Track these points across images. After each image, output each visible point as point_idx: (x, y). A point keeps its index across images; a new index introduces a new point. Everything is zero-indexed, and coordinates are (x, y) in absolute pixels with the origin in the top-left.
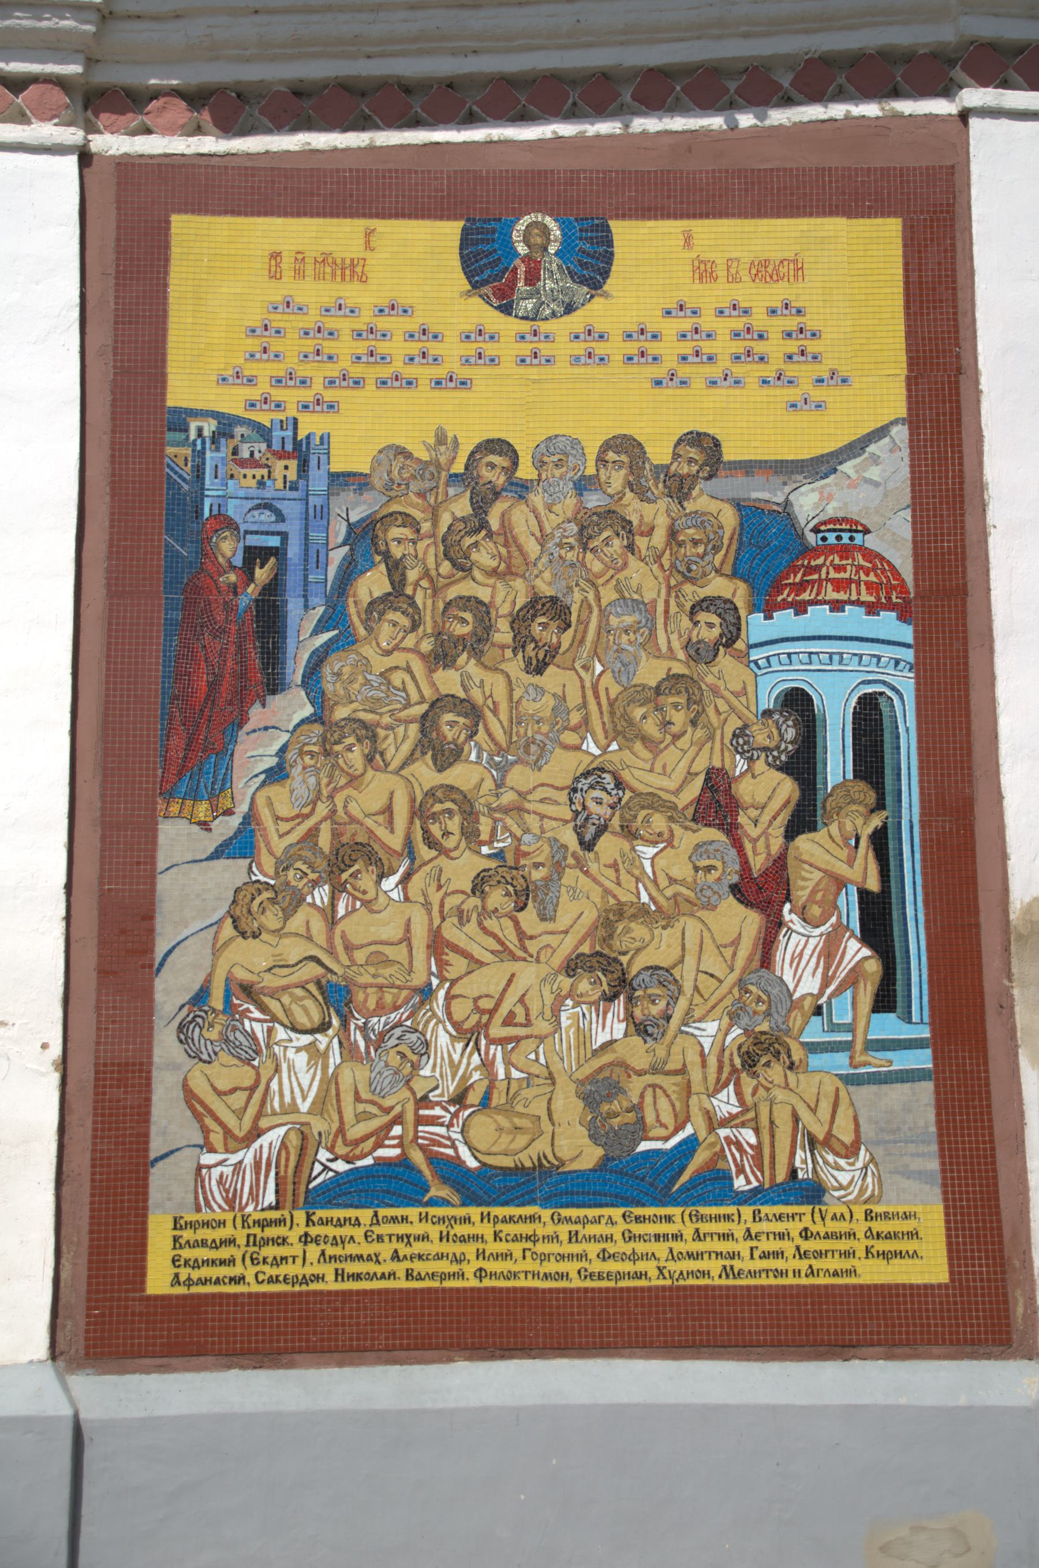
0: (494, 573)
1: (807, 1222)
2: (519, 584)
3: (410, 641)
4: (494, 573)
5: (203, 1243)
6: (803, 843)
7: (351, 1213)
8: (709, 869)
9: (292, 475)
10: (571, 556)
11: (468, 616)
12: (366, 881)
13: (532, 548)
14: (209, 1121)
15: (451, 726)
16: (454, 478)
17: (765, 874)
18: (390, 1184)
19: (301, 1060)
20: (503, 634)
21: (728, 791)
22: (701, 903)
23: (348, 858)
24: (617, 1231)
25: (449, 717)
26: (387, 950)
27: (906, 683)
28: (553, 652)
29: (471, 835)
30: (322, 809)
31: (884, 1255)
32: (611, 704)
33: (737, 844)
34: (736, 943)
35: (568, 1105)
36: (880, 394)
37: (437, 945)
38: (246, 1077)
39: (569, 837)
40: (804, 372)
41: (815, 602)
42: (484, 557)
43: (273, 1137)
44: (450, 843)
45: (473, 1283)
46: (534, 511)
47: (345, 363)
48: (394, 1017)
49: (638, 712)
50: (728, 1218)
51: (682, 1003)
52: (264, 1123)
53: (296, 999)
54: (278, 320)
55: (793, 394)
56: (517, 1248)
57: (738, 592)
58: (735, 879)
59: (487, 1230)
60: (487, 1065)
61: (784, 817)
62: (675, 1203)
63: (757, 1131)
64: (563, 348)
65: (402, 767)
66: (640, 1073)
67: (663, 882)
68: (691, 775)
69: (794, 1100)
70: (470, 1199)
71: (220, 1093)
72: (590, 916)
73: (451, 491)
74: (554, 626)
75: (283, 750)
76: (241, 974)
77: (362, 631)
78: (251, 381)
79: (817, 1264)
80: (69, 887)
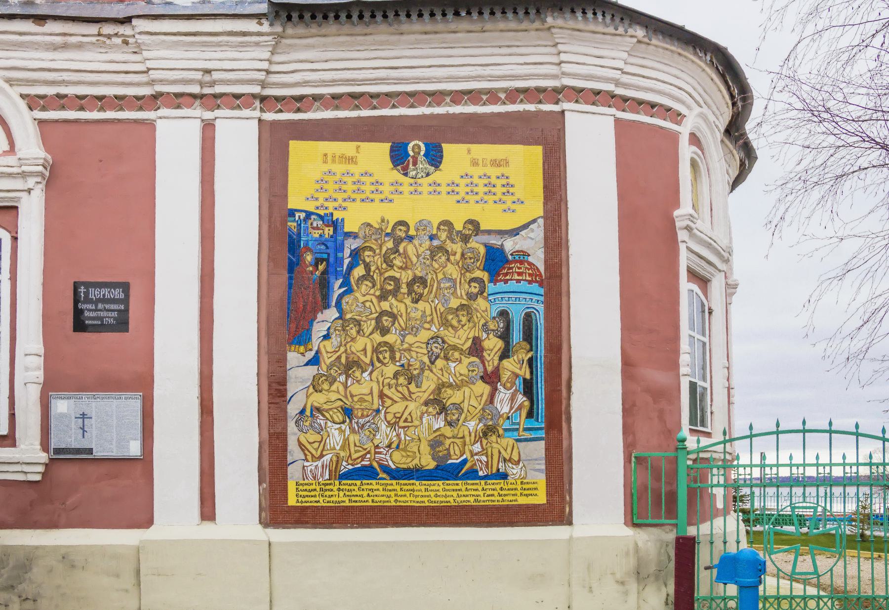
0: (401, 268)
1: (502, 485)
2: (409, 272)
3: (372, 291)
4: (401, 268)
5: (306, 490)
6: (505, 362)
7: (354, 482)
8: (473, 371)
9: (331, 233)
10: (428, 262)
11: (392, 283)
12: (358, 374)
13: (414, 259)
14: (306, 452)
15: (386, 321)
16: (387, 235)
17: (492, 372)
18: (367, 473)
19: (336, 433)
20: (404, 289)
21: (480, 345)
22: (471, 382)
23: (351, 366)
24: (440, 488)
25: (385, 318)
26: (365, 397)
27: (541, 307)
28: (421, 295)
29: (393, 358)
30: (342, 349)
31: (526, 495)
32: (441, 314)
33: (483, 362)
34: (481, 396)
35: (425, 448)
36: (534, 207)
37: (382, 395)
38: (318, 438)
39: (426, 359)
40: (509, 199)
41: (511, 280)
42: (398, 262)
43: (327, 458)
44: (386, 361)
45: (394, 504)
46: (415, 246)
47: (349, 193)
48: (367, 419)
49: (450, 317)
50: (477, 484)
51: (463, 416)
52: (324, 453)
53: (334, 413)
54: (326, 178)
55: (505, 207)
56: (408, 493)
57: (485, 276)
58: (482, 374)
59: (398, 488)
60: (398, 435)
61: (499, 353)
62: (460, 479)
63: (487, 457)
64: (425, 189)
65: (370, 334)
66: (449, 438)
67: (458, 375)
68: (468, 339)
69: (499, 447)
70: (393, 478)
71: (310, 443)
72: (433, 387)
73: (386, 239)
74: (421, 287)
75: (329, 328)
76: (316, 404)
77: (356, 288)
78: (317, 199)
79: (505, 498)
80: (258, 374)
